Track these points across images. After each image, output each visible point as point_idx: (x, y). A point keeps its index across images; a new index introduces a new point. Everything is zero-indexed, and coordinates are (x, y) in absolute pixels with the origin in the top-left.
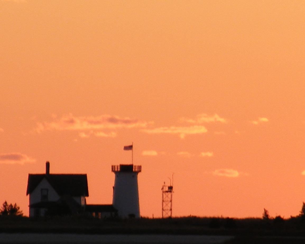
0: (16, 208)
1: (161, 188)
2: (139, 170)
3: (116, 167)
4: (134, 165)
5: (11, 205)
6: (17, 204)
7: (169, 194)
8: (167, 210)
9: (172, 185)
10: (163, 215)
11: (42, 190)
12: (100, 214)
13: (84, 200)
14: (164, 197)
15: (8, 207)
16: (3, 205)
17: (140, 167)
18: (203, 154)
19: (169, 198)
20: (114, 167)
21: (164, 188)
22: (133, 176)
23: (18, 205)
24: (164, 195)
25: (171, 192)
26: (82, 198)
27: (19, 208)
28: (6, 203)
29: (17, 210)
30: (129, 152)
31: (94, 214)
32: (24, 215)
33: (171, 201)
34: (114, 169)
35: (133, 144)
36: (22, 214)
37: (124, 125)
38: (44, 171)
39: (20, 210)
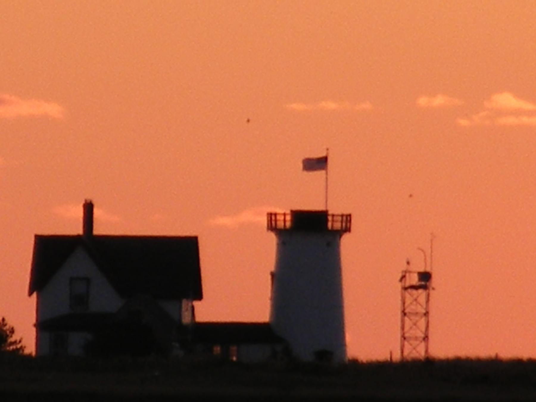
0: (5, 331)
1: (400, 276)
2: (344, 224)
3: (280, 218)
4: (330, 212)
8: (416, 338)
9: (428, 269)
10: (402, 352)
11: (87, 280)
13: (190, 309)
17: (348, 218)
18: (423, 101)
19: (422, 306)
20: (273, 218)
21: (407, 275)
22: (328, 244)
24: (407, 295)
25: (425, 287)
26: (185, 303)
27: (12, 331)
30: (320, 174)
32: (27, 351)
33: (426, 314)
34: (273, 223)
35: (327, 153)
36: (22, 348)
38: (78, 230)
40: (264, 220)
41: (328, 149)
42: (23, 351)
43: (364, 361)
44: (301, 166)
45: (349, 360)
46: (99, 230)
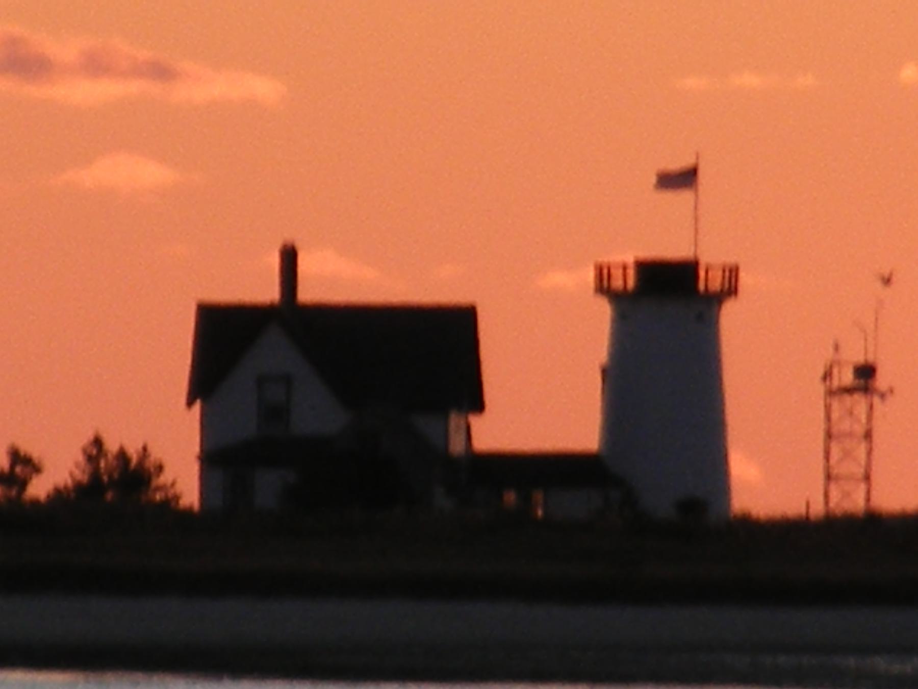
1: (821, 372)
2: (727, 286)
3: (617, 274)
4: (704, 260)
5: (122, 455)
6: (149, 448)
7: (859, 403)
8: (851, 435)
9: (871, 358)
10: (827, 502)
11: (287, 380)
12: (538, 496)
13: (464, 427)
14: (835, 415)
15: (106, 464)
16: (84, 451)
17: (732, 273)
19: (859, 421)
20: (605, 271)
21: (835, 371)
22: (700, 317)
23: (156, 453)
24: (836, 405)
25: (867, 390)
26: (455, 421)
27: (160, 468)
28: (98, 442)
29: (149, 481)
30: (682, 199)
31: (511, 497)
36: (177, 498)
37: (133, 87)
39: (165, 478)
40: (590, 276)
42: (177, 502)
44: (653, 179)
45: (735, 517)
46: (307, 294)
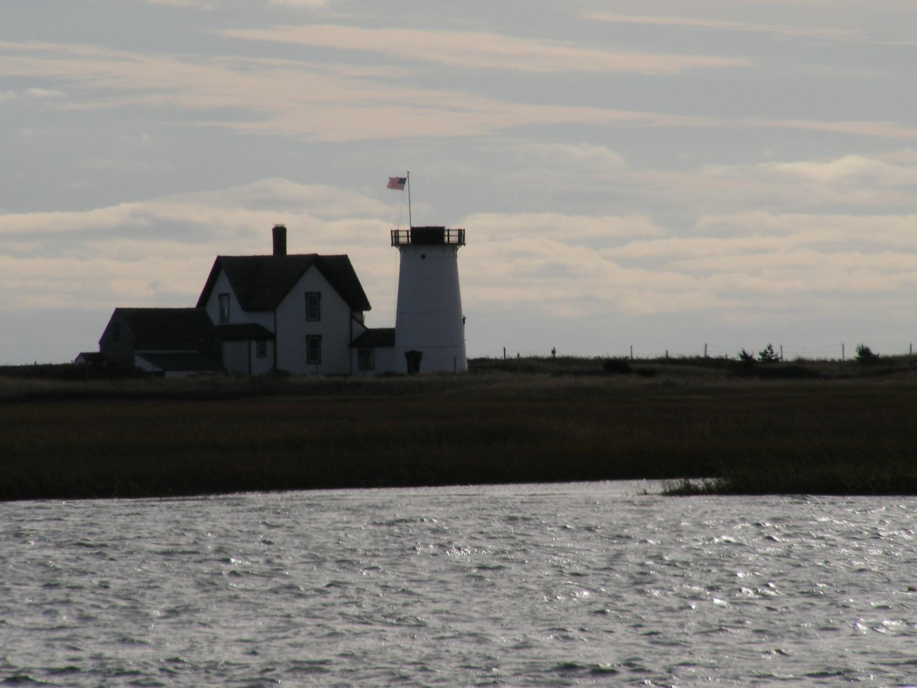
4: (446, 228)
17: (461, 233)
38: (266, 249)
41: (408, 173)
43: (688, 357)
46: (293, 248)
